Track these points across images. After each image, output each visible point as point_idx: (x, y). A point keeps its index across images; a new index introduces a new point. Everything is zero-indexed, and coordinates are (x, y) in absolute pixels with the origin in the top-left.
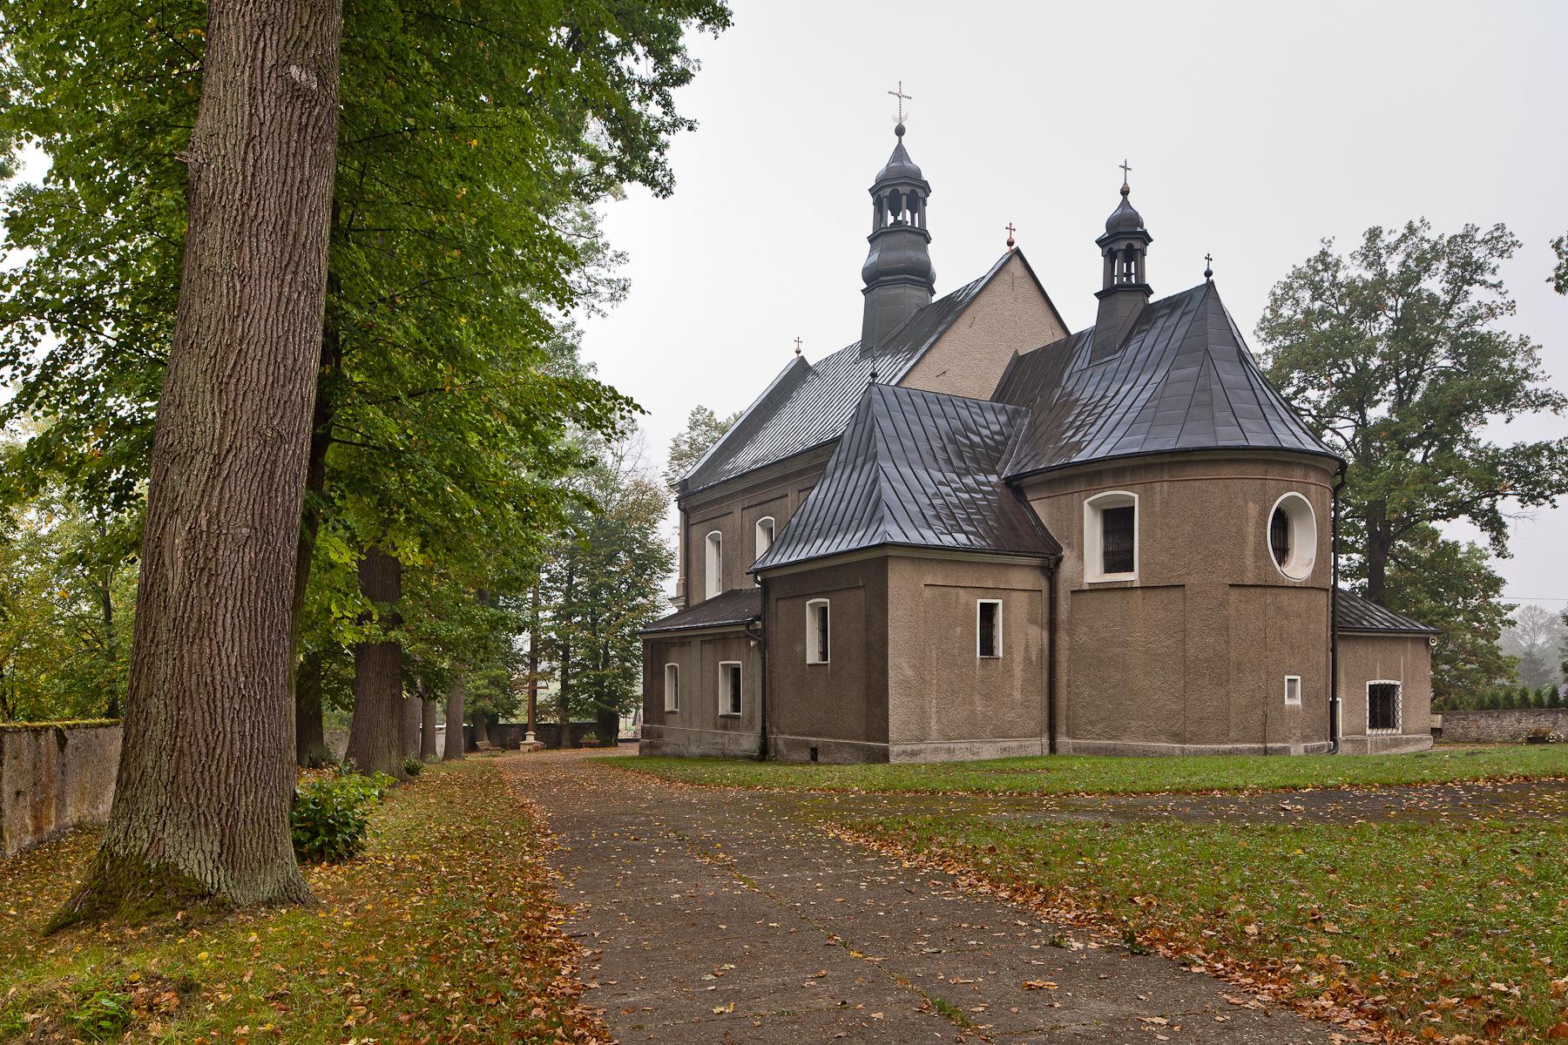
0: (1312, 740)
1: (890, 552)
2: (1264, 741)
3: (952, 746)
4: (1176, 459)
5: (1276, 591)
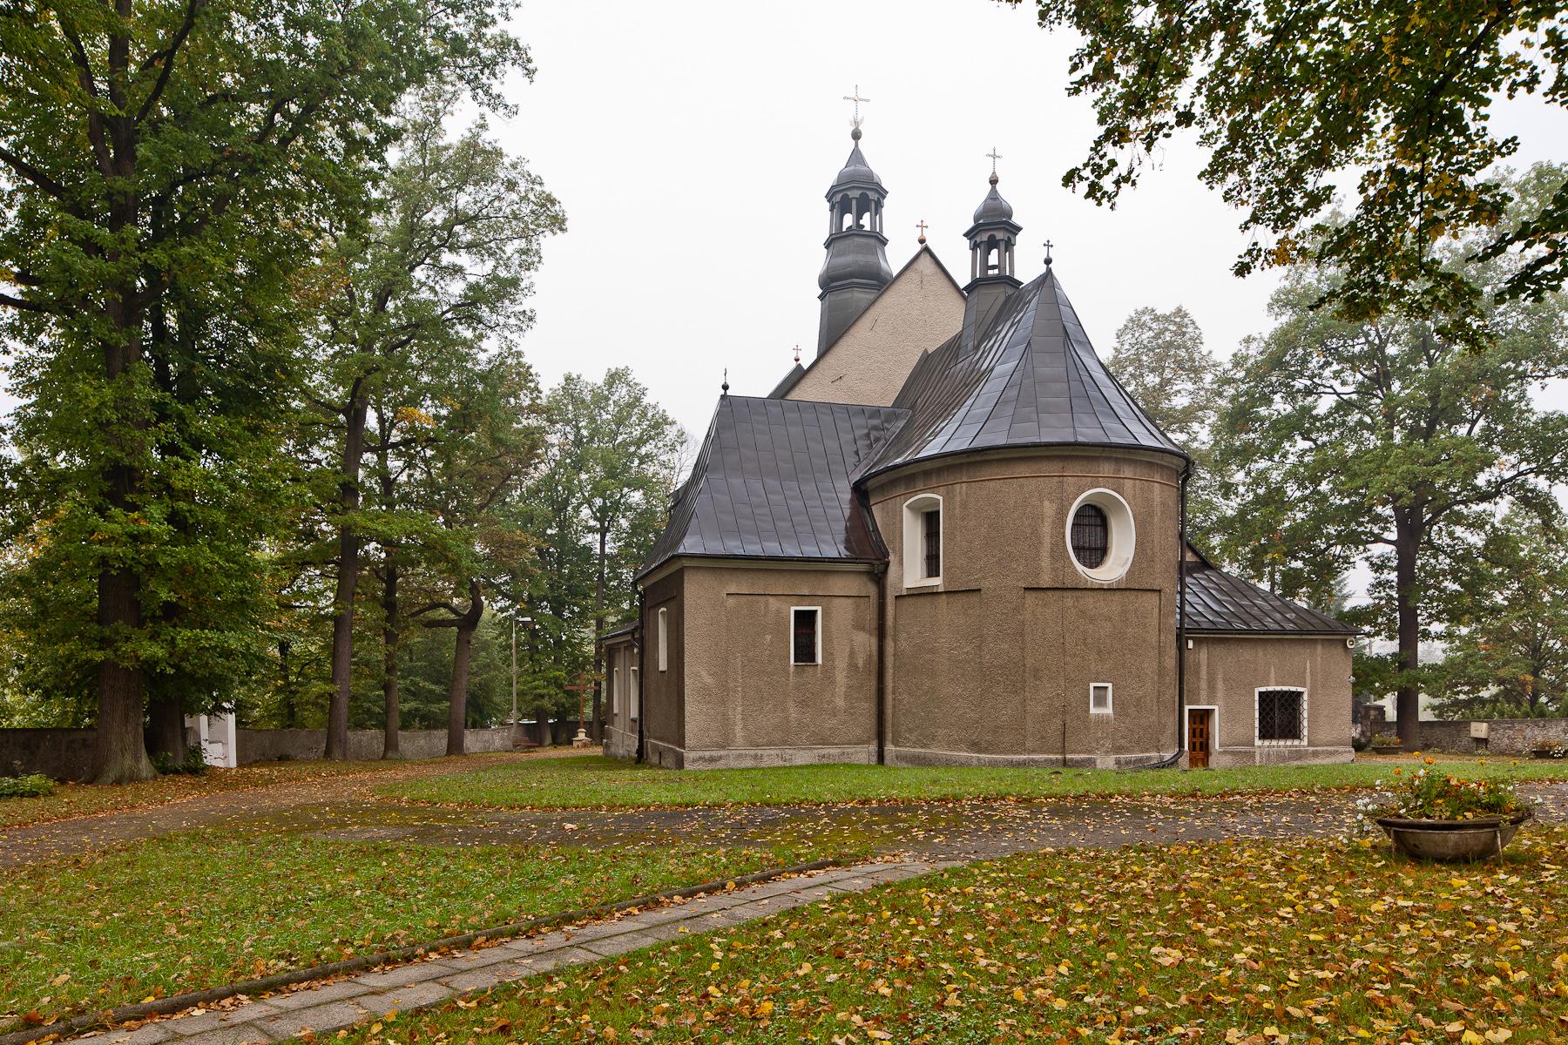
0: (1128, 751)
1: (686, 563)
2: (1063, 753)
3: (759, 752)
4: (972, 459)
5: (1079, 593)
